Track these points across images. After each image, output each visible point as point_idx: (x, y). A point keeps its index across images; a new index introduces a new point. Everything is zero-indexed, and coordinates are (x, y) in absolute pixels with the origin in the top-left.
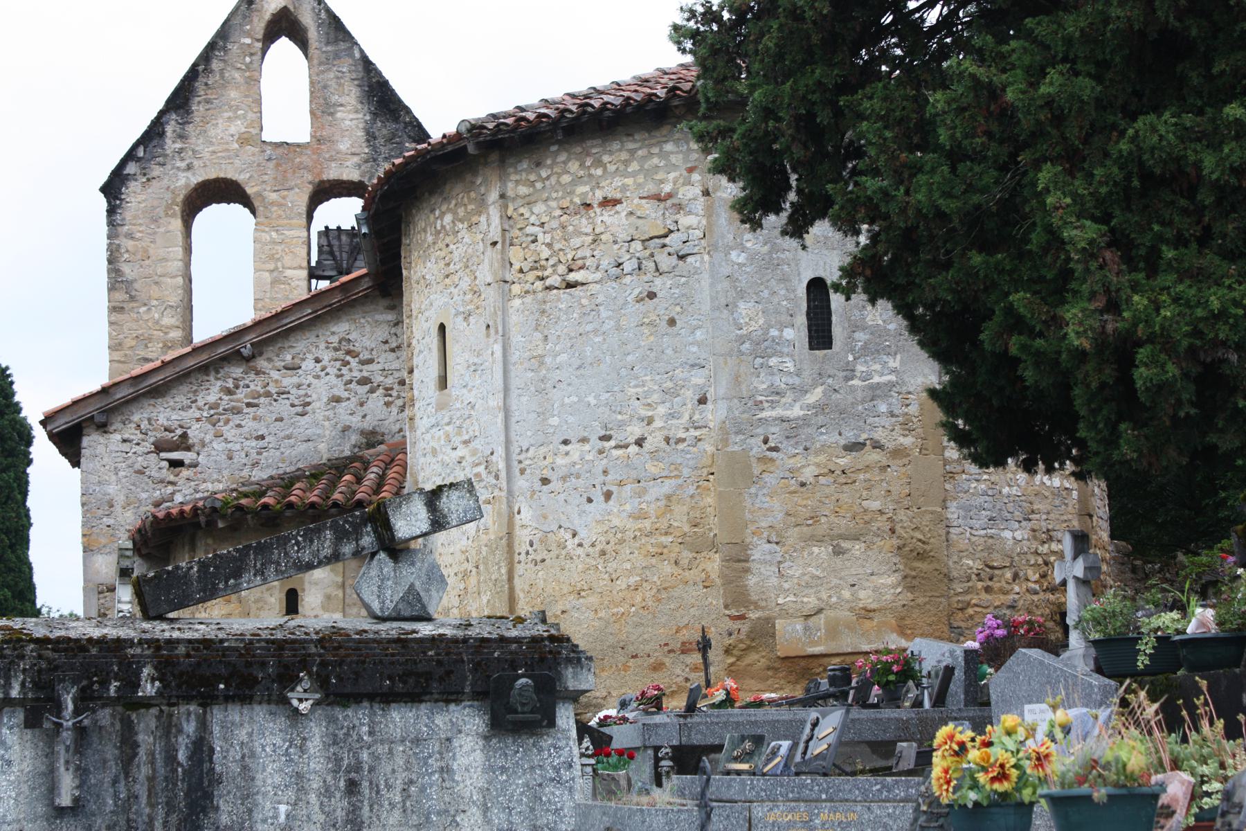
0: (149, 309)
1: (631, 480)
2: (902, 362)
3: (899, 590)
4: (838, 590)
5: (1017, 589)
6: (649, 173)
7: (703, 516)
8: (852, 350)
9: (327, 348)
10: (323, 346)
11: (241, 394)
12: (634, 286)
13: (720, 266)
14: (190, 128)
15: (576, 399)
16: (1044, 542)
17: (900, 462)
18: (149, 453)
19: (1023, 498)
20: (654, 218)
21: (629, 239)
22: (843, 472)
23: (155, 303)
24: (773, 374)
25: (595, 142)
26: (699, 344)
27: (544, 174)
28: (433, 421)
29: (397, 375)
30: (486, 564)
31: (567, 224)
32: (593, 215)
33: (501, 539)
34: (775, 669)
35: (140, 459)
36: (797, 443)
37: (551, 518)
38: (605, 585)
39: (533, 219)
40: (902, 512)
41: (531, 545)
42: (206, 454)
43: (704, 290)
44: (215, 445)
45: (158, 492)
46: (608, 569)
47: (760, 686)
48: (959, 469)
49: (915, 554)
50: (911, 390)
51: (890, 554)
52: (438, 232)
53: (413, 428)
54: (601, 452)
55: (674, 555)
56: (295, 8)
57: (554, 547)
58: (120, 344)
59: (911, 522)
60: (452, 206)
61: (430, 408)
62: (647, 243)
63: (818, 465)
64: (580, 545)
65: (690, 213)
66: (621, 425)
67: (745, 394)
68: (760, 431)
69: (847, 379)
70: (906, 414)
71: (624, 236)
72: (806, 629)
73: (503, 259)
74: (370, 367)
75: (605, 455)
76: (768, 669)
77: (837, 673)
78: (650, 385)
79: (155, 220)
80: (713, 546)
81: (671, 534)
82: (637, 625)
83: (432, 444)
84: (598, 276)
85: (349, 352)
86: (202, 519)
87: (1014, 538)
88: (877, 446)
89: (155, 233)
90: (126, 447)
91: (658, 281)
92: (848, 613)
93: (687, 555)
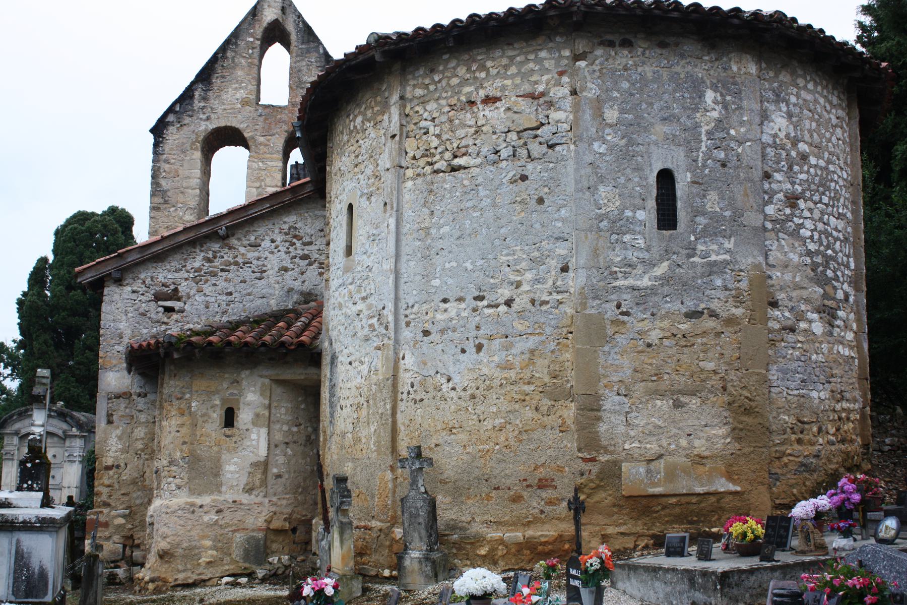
0: (176, 209)
1: (499, 335)
2: (735, 244)
3: (728, 440)
4: (676, 439)
5: (821, 441)
6: (525, 76)
8: (694, 232)
9: (280, 232)
10: (277, 231)
11: (217, 263)
12: (509, 170)
13: (584, 154)
14: (210, 93)
15: (455, 264)
16: (839, 401)
17: (730, 329)
19: (826, 364)
20: (529, 113)
21: (506, 130)
22: (684, 336)
23: (180, 205)
24: (626, 249)
25: (480, 51)
26: (563, 220)
27: (437, 78)
28: (341, 281)
30: (375, 400)
31: (455, 118)
32: (476, 110)
33: (388, 380)
34: (620, 506)
35: (143, 305)
36: (645, 309)
37: (430, 364)
38: (474, 425)
39: (426, 115)
40: (733, 372)
42: (190, 303)
43: (569, 174)
45: (155, 329)
46: (476, 411)
47: (606, 521)
48: (779, 338)
49: (742, 409)
50: (743, 268)
51: (721, 409)
52: (351, 132)
53: (327, 287)
54: (474, 310)
56: (283, 20)
57: (431, 389)
58: (156, 231)
59: (740, 381)
60: (362, 109)
61: (339, 272)
62: (521, 134)
63: (662, 329)
64: (454, 389)
65: (559, 109)
66: (493, 287)
67: (602, 265)
68: (613, 297)
69: (689, 256)
71: (501, 128)
72: (648, 471)
73: (400, 149)
74: (310, 248)
75: (478, 312)
76: (614, 506)
77: (785, 600)
78: (520, 254)
79: (184, 152)
80: (570, 396)
81: (533, 383)
82: (500, 461)
83: (339, 300)
84: (478, 161)
85: (295, 237)
86: (161, 351)
87: (819, 398)
88: (713, 314)
89: (183, 160)
90: (134, 296)
91: (530, 166)
92: (684, 459)
93: (546, 403)
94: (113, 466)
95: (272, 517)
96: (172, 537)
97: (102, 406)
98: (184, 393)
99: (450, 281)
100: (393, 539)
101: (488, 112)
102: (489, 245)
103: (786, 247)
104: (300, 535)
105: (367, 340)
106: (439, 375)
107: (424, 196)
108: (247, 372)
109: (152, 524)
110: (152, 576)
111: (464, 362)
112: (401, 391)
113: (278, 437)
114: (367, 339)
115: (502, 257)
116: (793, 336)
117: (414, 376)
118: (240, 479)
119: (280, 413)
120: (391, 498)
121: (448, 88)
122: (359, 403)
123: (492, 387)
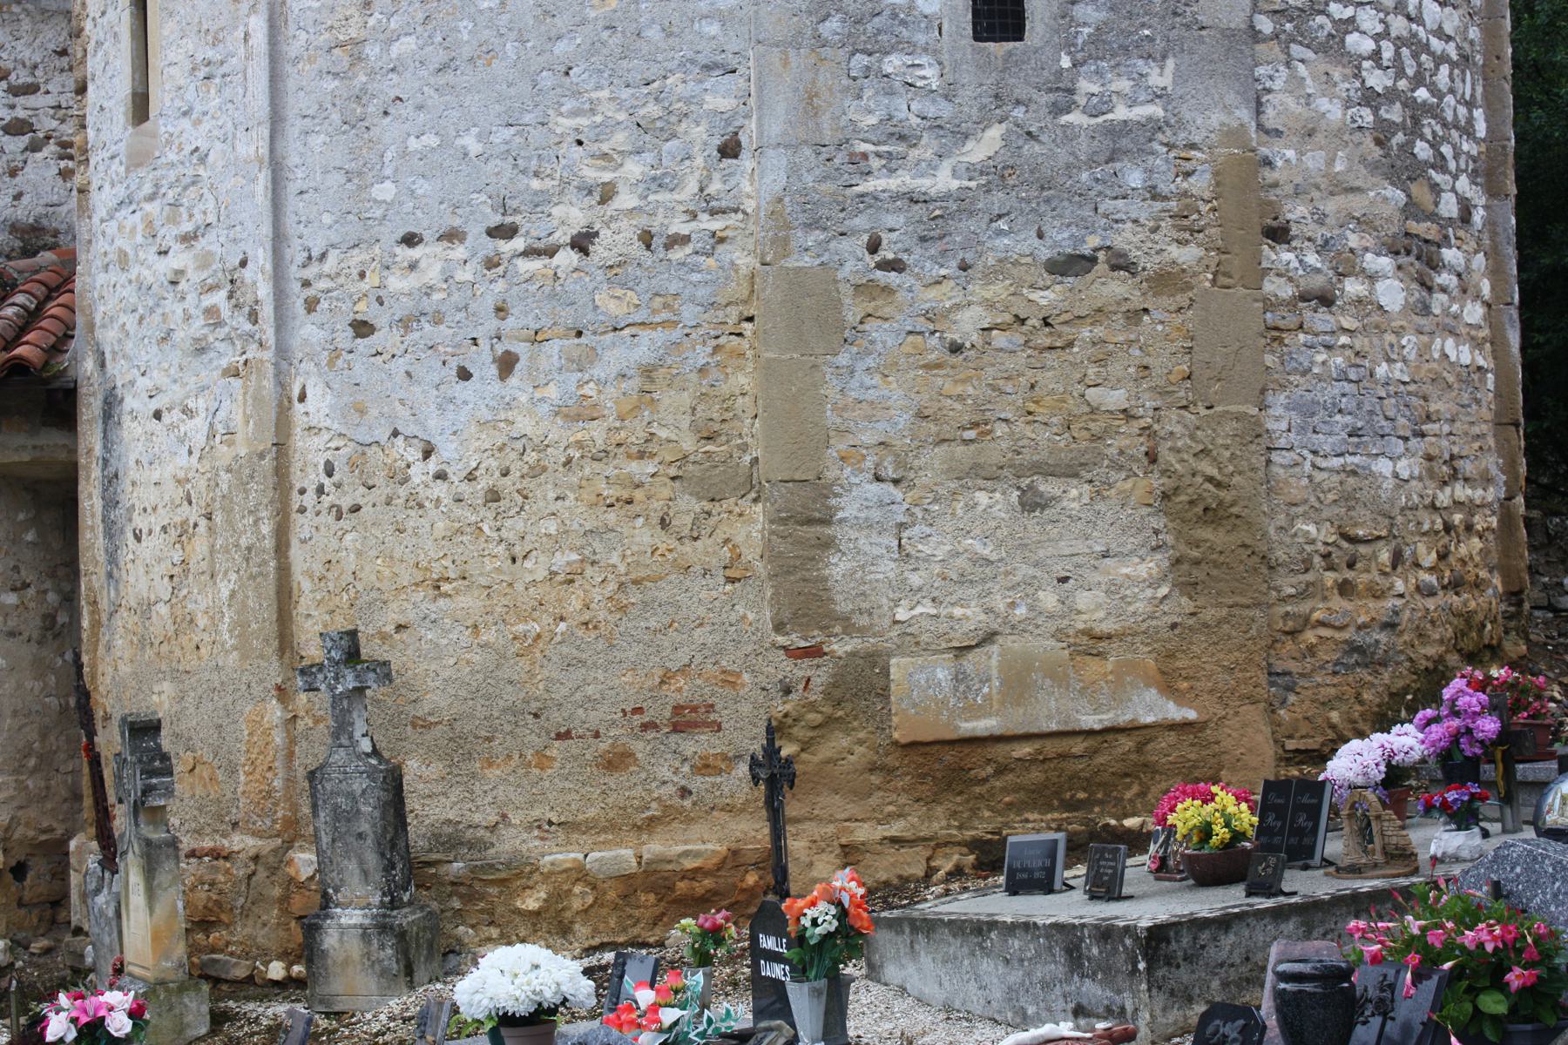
1: (560, 330)
2: (1177, 74)
3: (1164, 590)
4: (1030, 590)
5: (1400, 586)
7: (728, 415)
8: (1069, 45)
16: (1445, 483)
17: (1165, 301)
19: (1412, 388)
22: (1046, 322)
24: (891, 93)
28: (121, 191)
30: (228, 511)
33: (262, 456)
34: (889, 771)
37: (374, 412)
38: (498, 570)
40: (1174, 415)
41: (330, 474)
46: (504, 533)
47: (853, 809)
48: (1291, 321)
49: (1199, 510)
53: (84, 209)
54: (491, 264)
55: (656, 505)
57: (380, 479)
59: (1192, 437)
63: (990, 305)
64: (441, 476)
67: (828, 136)
68: (860, 222)
69: (1058, 110)
70: (1185, 194)
72: (959, 678)
74: (31, 101)
75: (500, 270)
77: (1308, 987)
78: (609, 109)
80: (751, 487)
87: (1396, 475)
88: (1121, 264)
92: (1052, 642)
93: (688, 506)
100: (291, 880)
102: (525, 87)
103: (1309, 81)
104: (36, 883)
105: (201, 351)
106: (400, 441)
111: (465, 403)
112: (298, 486)
114: (200, 349)
115: (561, 120)
116: (1328, 317)
117: (333, 445)
120: (281, 773)
123: (544, 469)
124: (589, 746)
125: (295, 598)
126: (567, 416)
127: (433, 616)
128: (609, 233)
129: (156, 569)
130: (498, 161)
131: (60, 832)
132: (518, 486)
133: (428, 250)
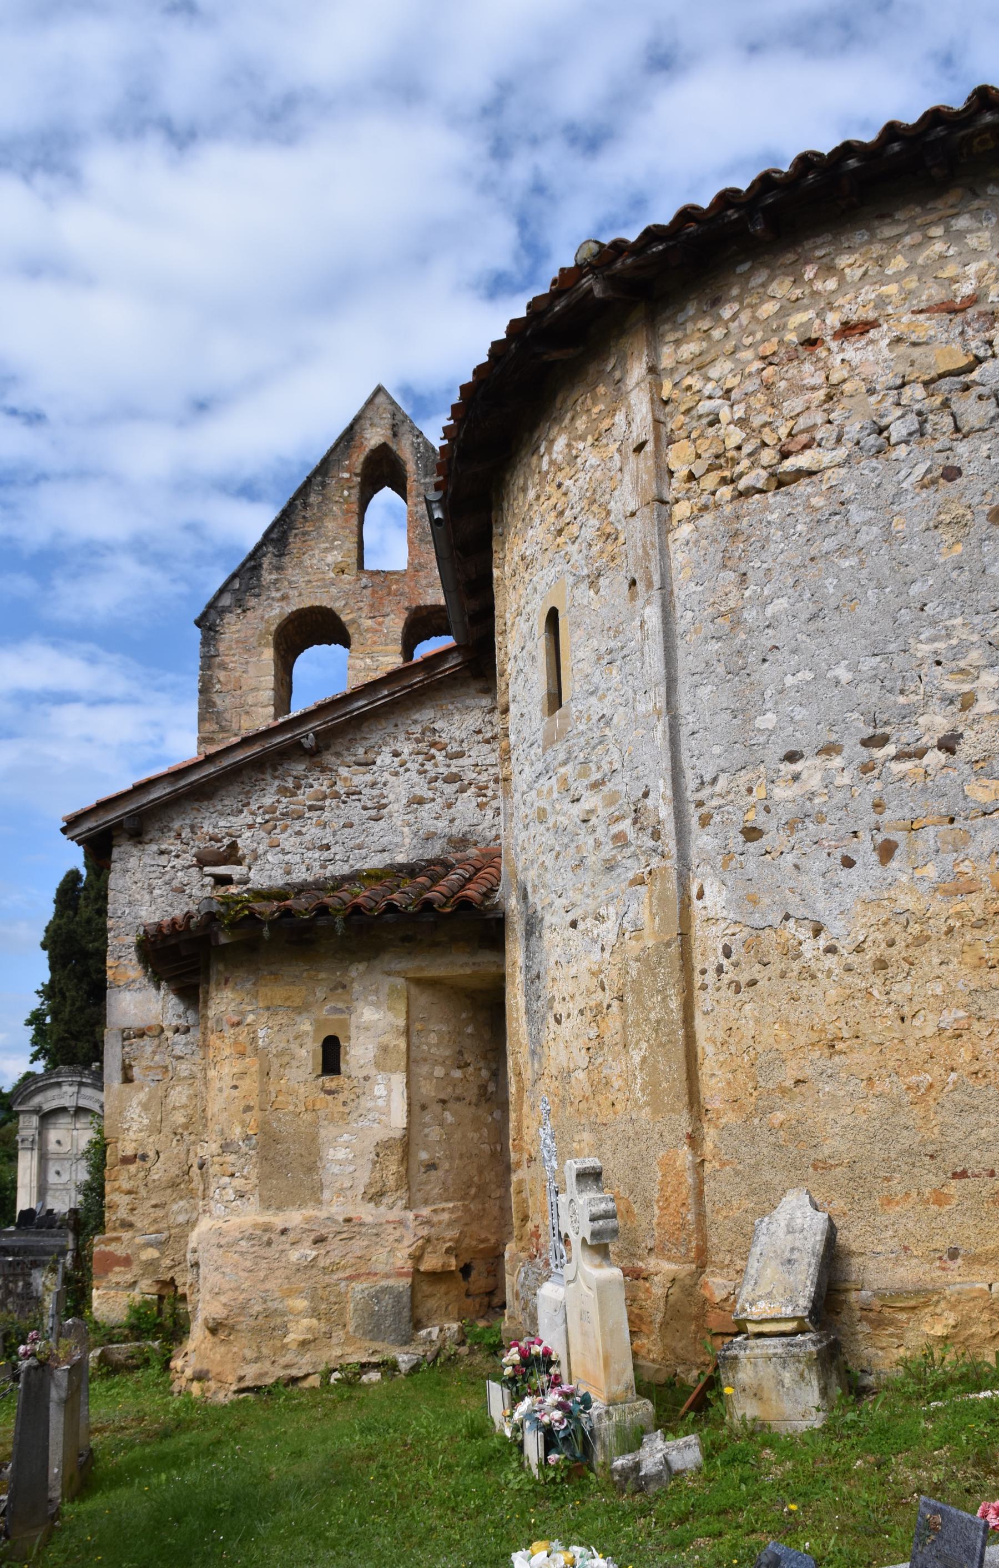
6: (923, 272)
14: (286, 559)
15: (809, 676)
18: (190, 866)
21: (899, 381)
25: (819, 241)
27: (727, 313)
28: (540, 766)
29: (492, 770)
30: (637, 992)
31: (776, 378)
32: (824, 354)
33: (668, 945)
35: (180, 874)
37: (766, 901)
39: (709, 388)
44: (269, 857)
46: (893, 996)
54: (866, 768)
57: (774, 957)
64: (831, 950)
71: (886, 379)
73: (658, 466)
74: (460, 762)
75: (876, 772)
78: (963, 634)
85: (433, 745)
89: (247, 663)
90: (163, 860)
91: (962, 448)
94: (135, 1156)
95: (423, 1249)
96: (230, 1293)
97: (113, 1054)
98: (243, 1014)
99: (800, 713)
100: (706, 1301)
101: (853, 351)
102: (887, 623)
104: (478, 1280)
105: (610, 869)
106: (791, 923)
107: (723, 545)
108: (362, 967)
109: (196, 1265)
110: (199, 1367)
111: (851, 886)
113: (427, 1090)
114: (610, 866)
115: (919, 646)
117: (729, 931)
118: (357, 1174)
119: (428, 1044)
120: (693, 1208)
121: (752, 327)
122: (599, 1005)
123: (928, 938)
124: (986, 1184)
125: (700, 1061)
126: (945, 891)
127: (830, 1071)
128: (972, 733)
129: (575, 1044)
130: (867, 685)
131: (493, 1241)
132: (904, 954)
133: (808, 763)
